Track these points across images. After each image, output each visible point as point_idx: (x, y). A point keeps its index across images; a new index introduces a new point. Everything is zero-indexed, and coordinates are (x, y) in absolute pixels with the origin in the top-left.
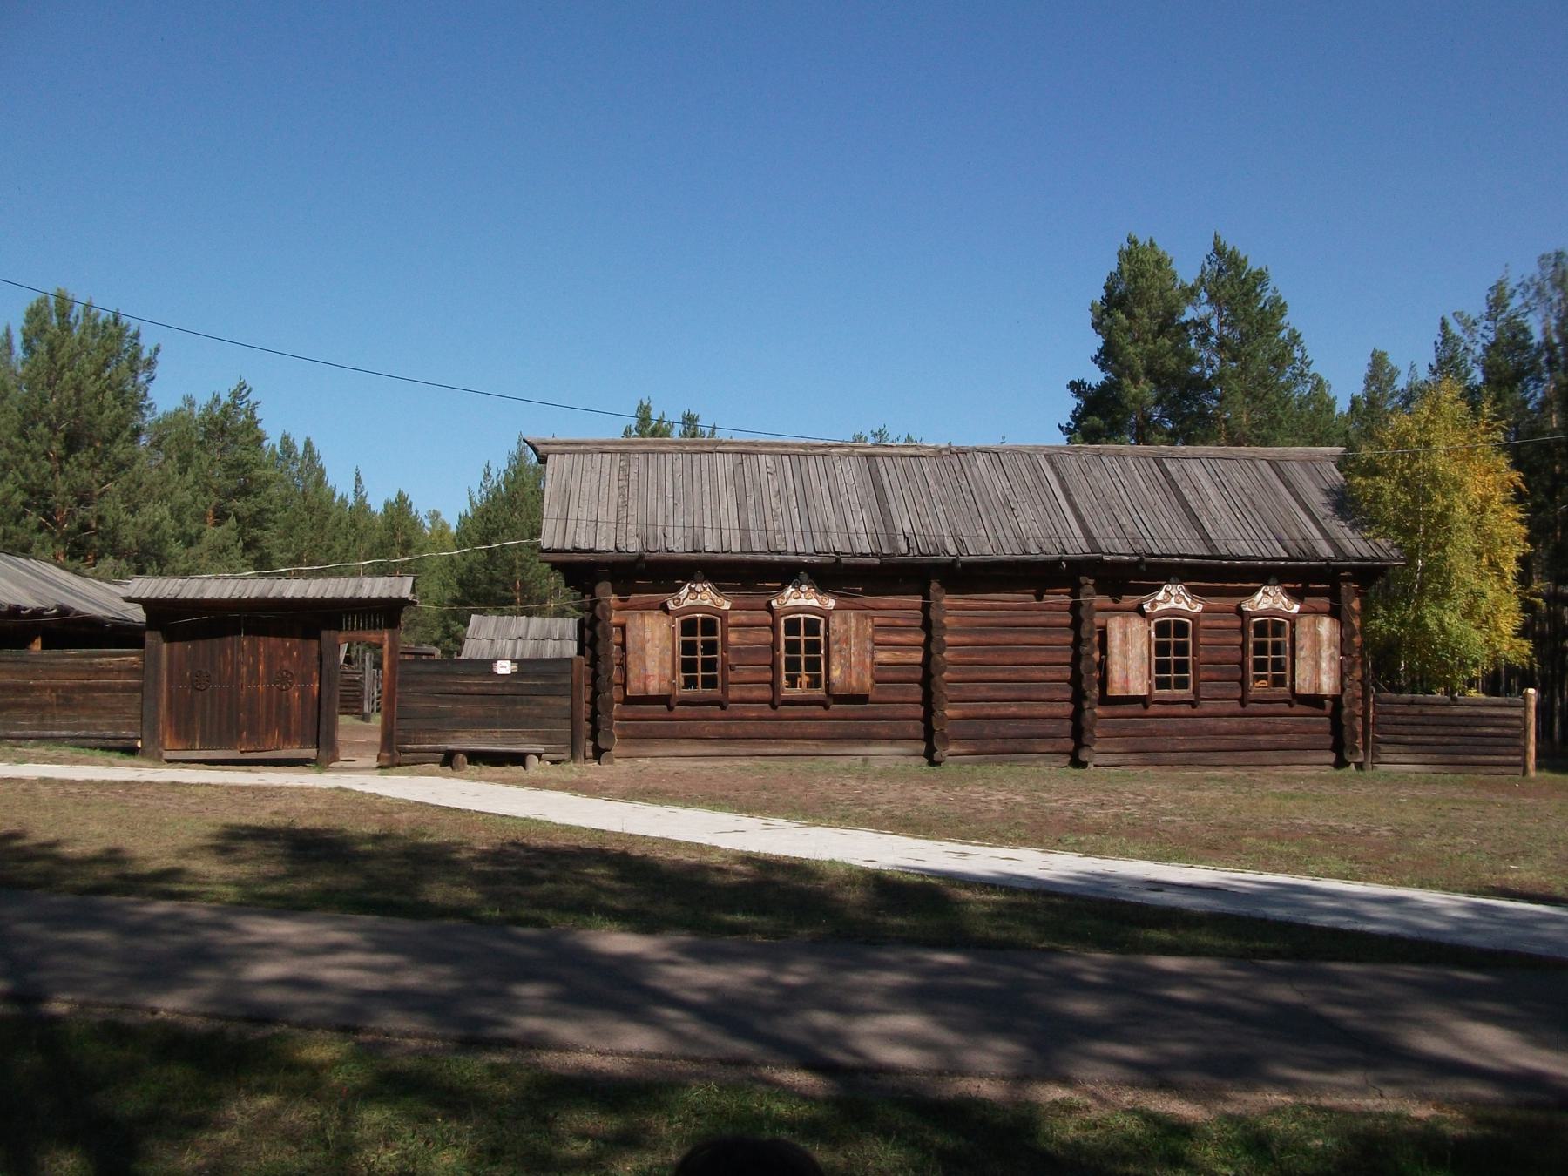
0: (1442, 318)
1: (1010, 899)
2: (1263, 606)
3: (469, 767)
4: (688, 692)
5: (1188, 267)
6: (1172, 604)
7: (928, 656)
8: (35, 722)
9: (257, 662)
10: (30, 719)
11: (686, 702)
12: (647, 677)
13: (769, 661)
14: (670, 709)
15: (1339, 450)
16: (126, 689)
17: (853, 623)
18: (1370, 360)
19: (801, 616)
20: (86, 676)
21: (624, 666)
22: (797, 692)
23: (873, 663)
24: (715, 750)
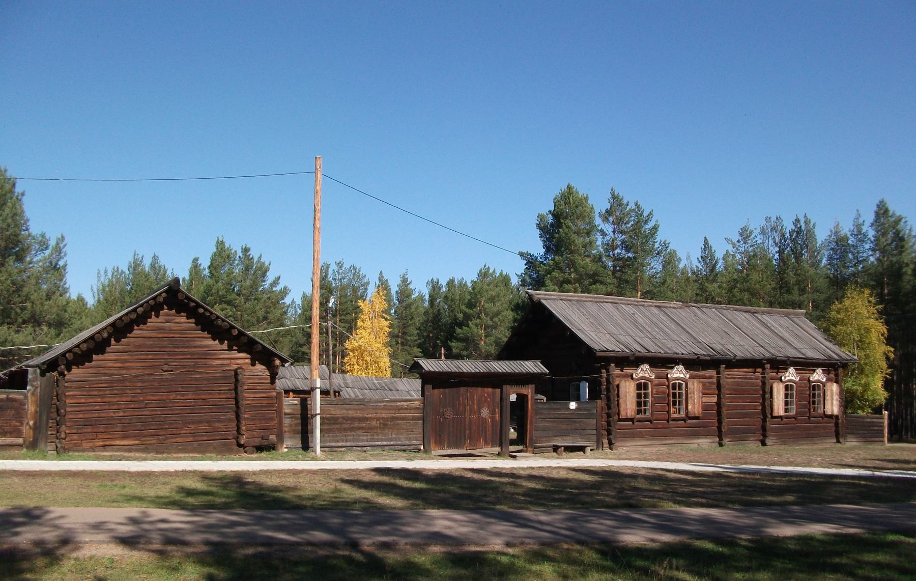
0: (705, 238)
1: (884, 485)
2: (816, 379)
3: (564, 453)
4: (639, 416)
5: (599, 203)
6: (791, 378)
7: (719, 398)
8: (369, 437)
9: (473, 403)
10: (367, 436)
11: (639, 421)
12: (627, 409)
13: (667, 402)
14: (782, 420)
15: (805, 311)
16: (414, 419)
17: (696, 384)
18: (538, 232)
19: (677, 381)
20: (393, 412)
21: (618, 405)
22: (676, 416)
23: (702, 402)
24: (649, 442)
